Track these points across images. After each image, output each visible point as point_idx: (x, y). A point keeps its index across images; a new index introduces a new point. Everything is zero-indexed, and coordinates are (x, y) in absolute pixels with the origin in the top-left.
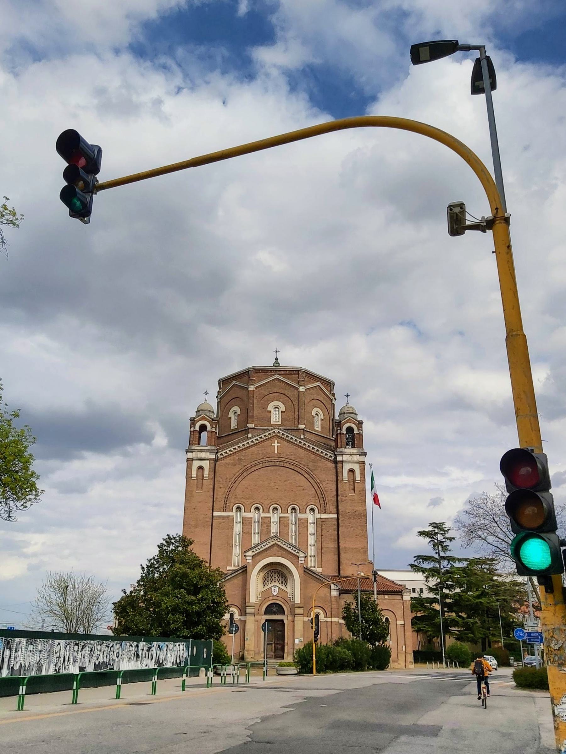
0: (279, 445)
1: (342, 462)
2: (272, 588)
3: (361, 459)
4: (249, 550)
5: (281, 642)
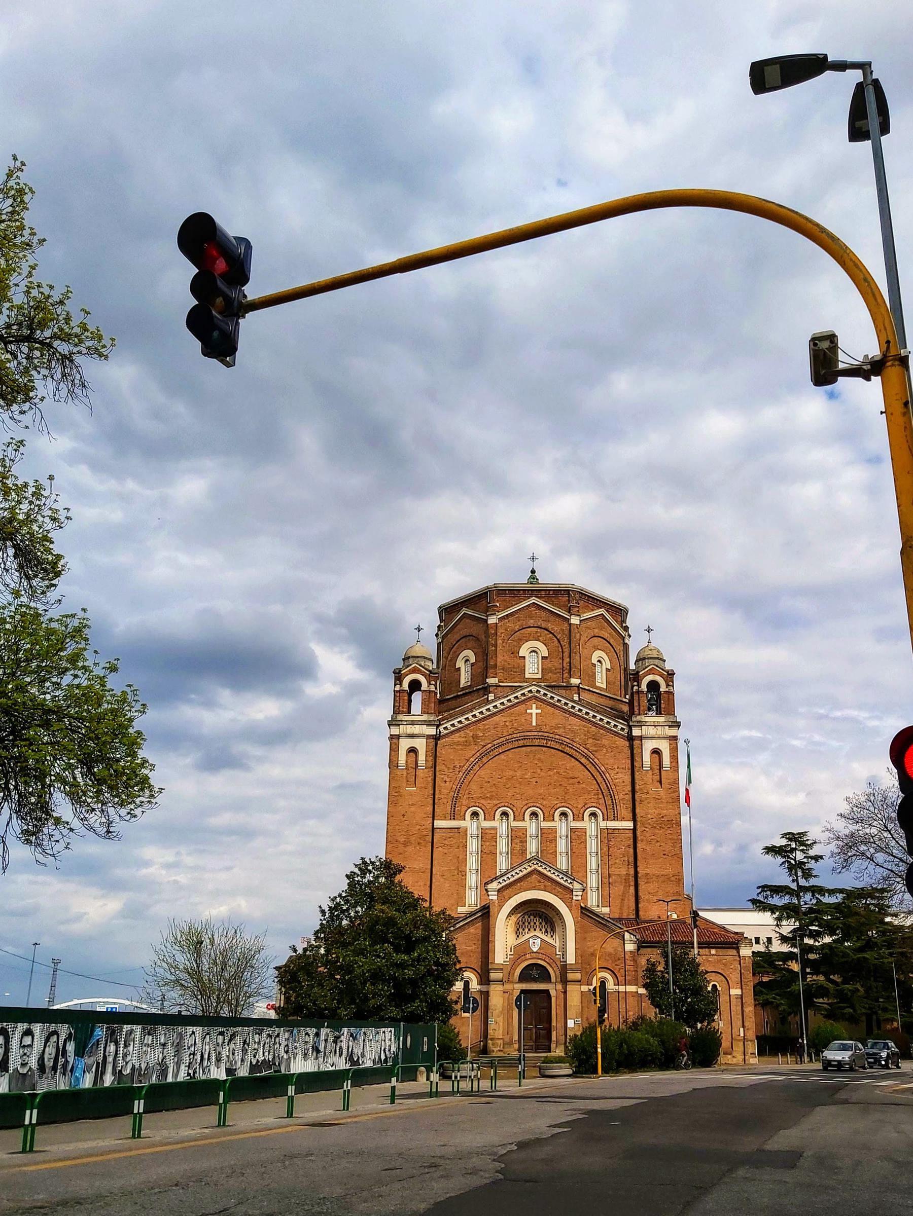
0: (539, 711)
1: (641, 738)
2: (530, 939)
3: (672, 732)
4: (492, 881)
5: (547, 1026)
